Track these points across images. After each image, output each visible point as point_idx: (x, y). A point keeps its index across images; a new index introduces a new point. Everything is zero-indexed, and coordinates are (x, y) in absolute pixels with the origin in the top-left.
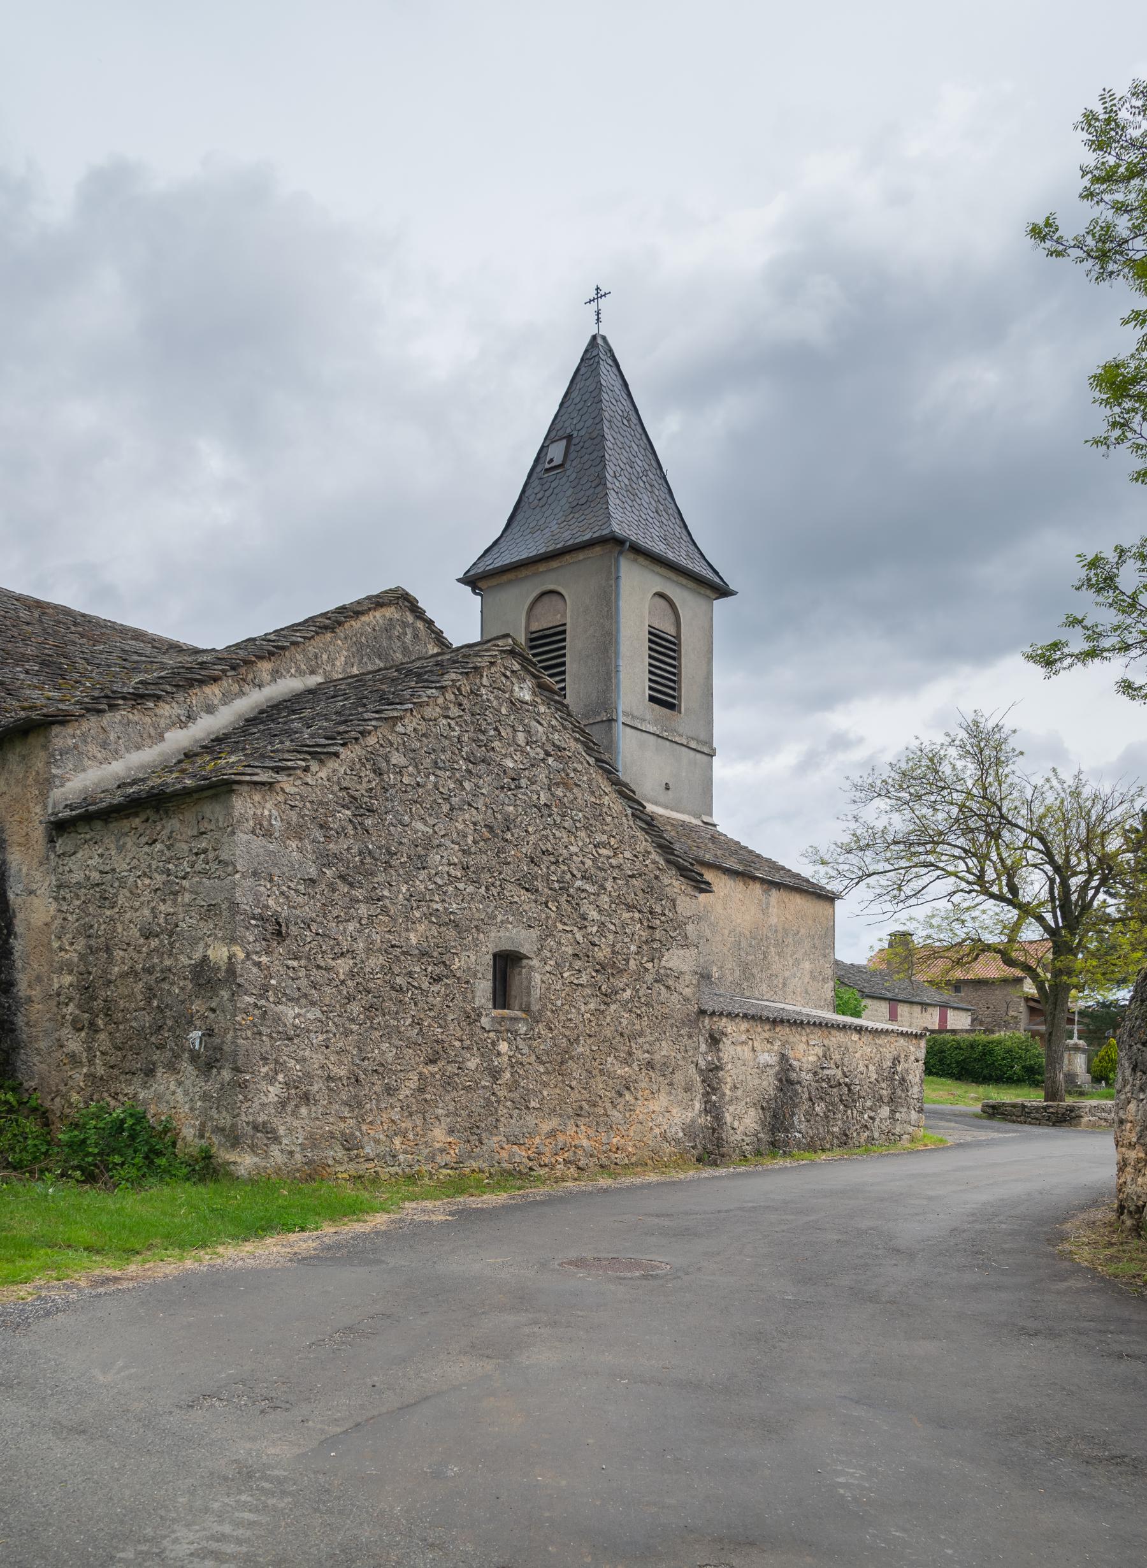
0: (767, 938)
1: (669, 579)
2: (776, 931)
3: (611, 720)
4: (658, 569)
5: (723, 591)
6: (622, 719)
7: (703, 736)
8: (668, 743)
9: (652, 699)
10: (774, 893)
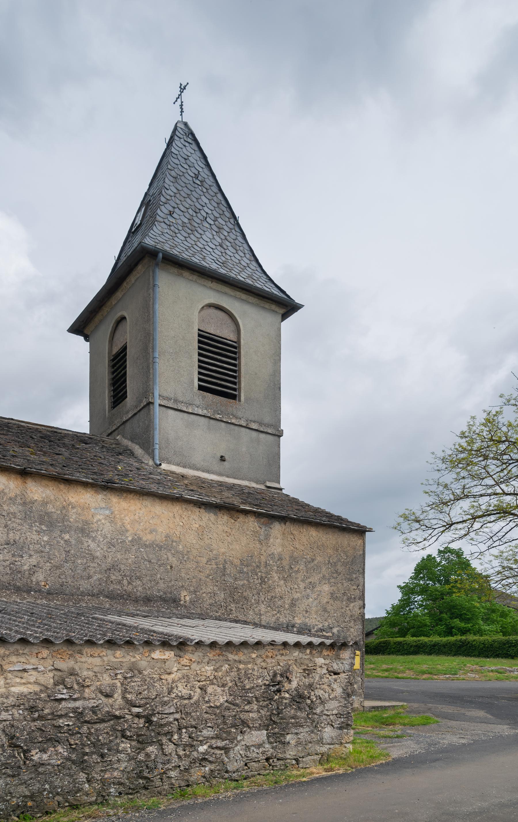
0: (266, 565)
1: (226, 293)
2: (280, 559)
3: (149, 404)
4: (209, 283)
5: (287, 307)
6: (158, 401)
7: (267, 419)
8: (223, 424)
9: (201, 388)
10: (277, 528)
